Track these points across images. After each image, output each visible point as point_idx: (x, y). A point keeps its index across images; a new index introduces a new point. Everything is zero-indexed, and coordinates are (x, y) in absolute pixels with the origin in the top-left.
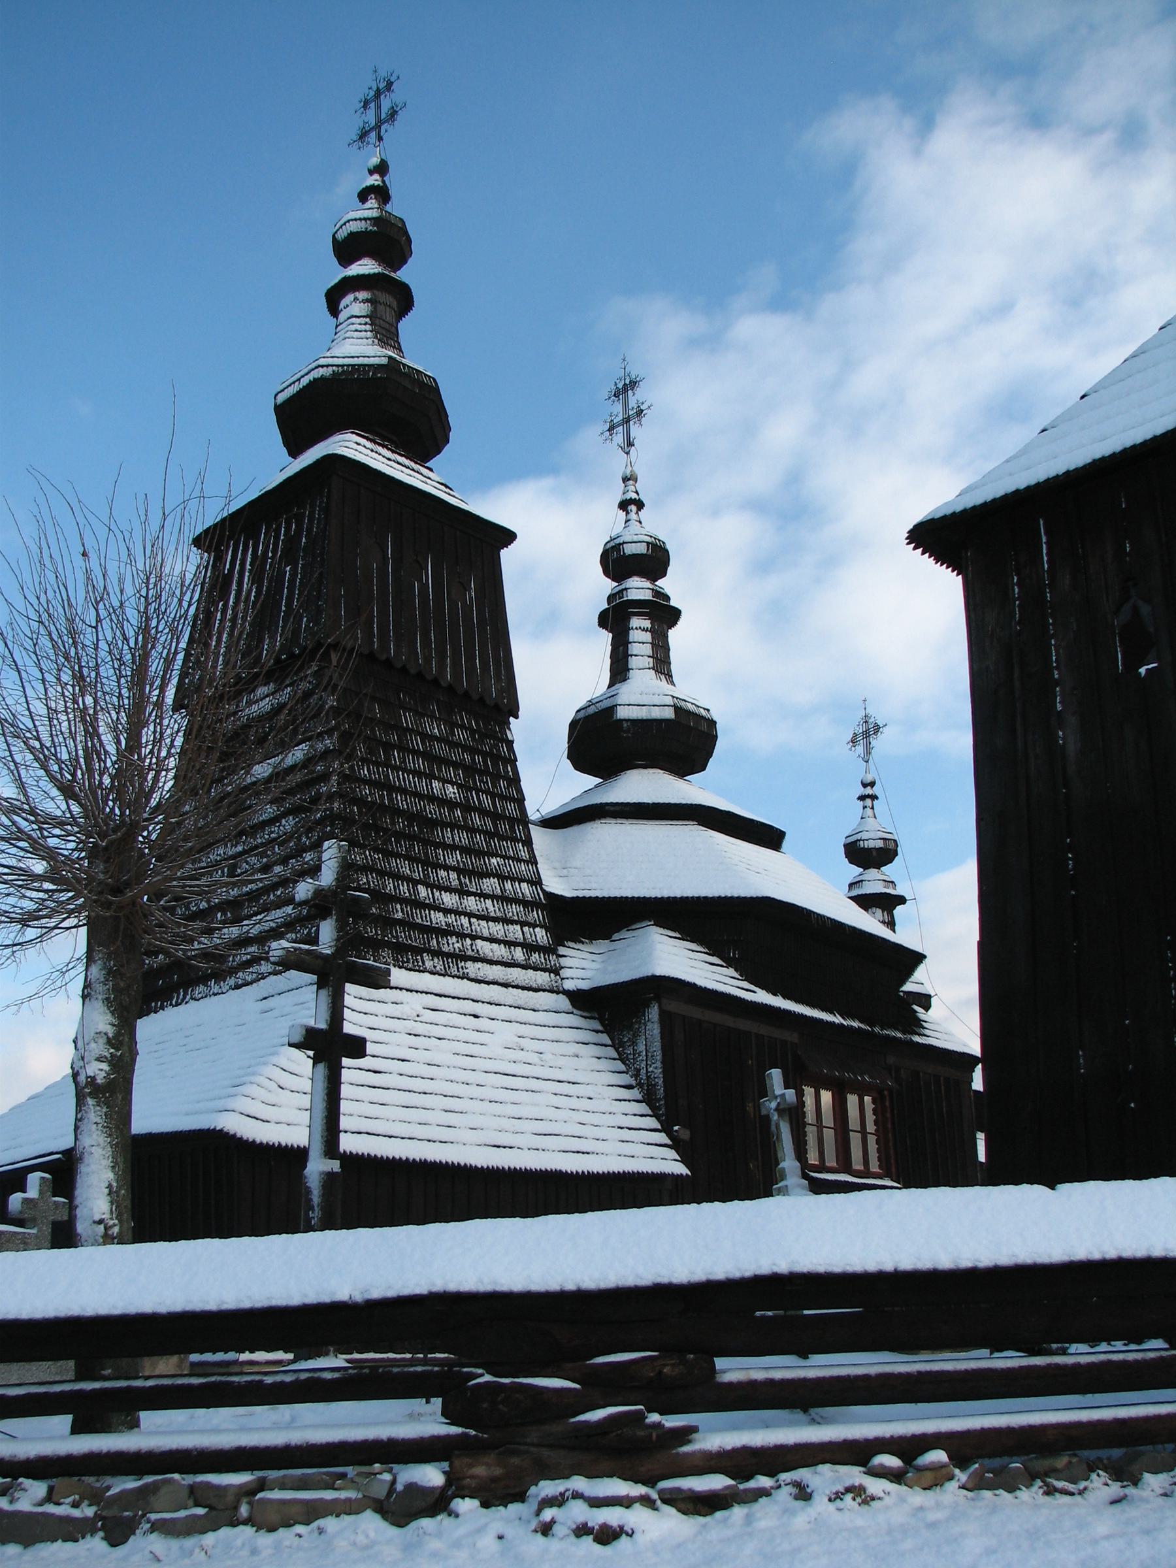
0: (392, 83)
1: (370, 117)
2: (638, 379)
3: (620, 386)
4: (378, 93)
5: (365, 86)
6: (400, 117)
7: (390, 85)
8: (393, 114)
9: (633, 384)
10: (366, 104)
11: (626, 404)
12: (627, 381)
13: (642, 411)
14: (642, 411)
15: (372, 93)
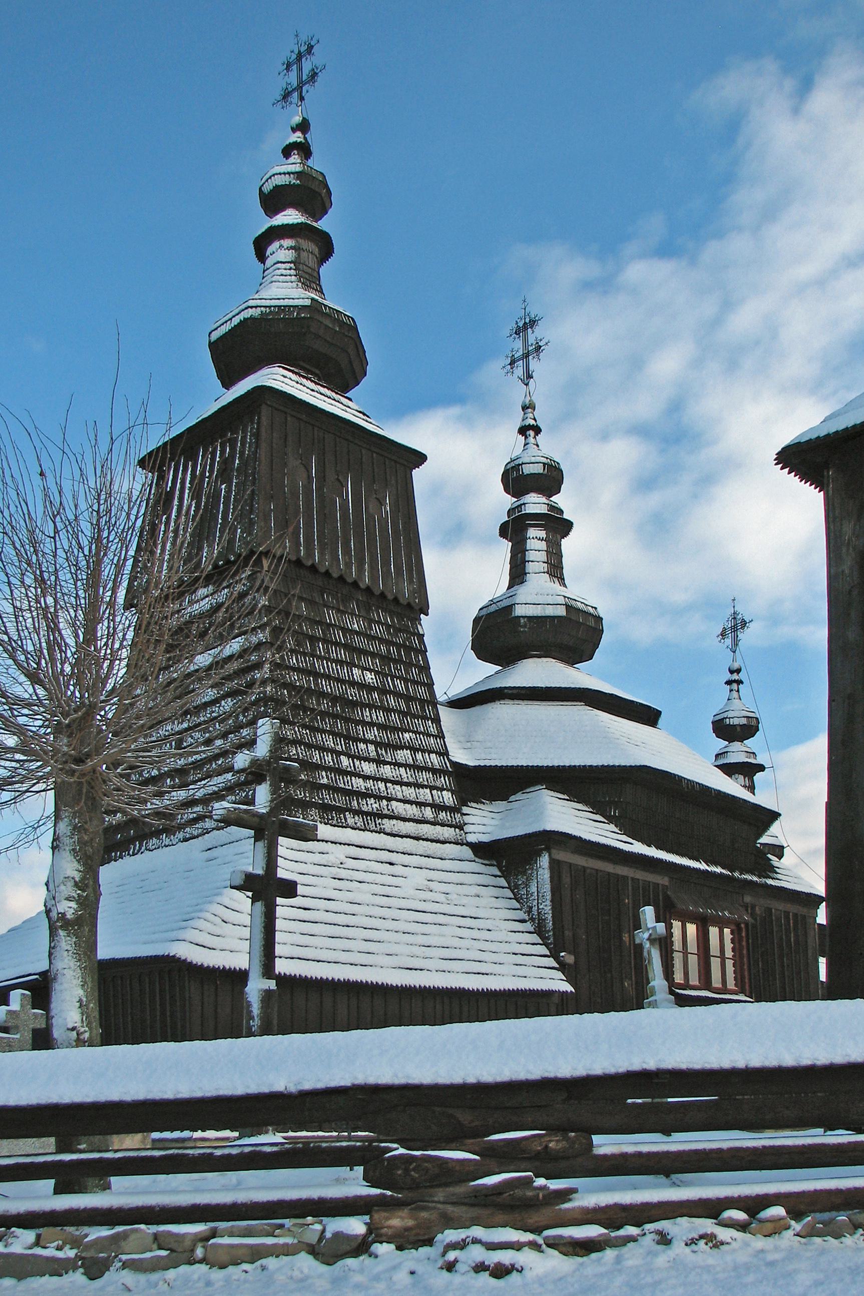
0: (312, 46)
1: (293, 78)
2: (537, 318)
3: (521, 324)
4: (300, 56)
5: (288, 49)
6: (320, 79)
7: (310, 48)
8: (313, 76)
9: (533, 323)
10: (288, 67)
11: (525, 341)
12: (527, 320)
13: (540, 347)
14: (540, 347)
15: (294, 56)
